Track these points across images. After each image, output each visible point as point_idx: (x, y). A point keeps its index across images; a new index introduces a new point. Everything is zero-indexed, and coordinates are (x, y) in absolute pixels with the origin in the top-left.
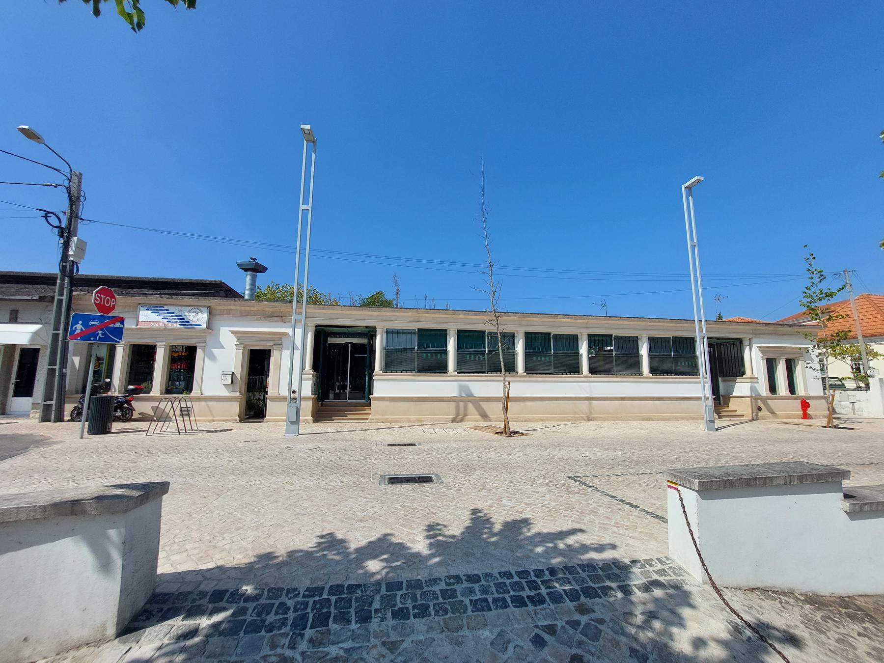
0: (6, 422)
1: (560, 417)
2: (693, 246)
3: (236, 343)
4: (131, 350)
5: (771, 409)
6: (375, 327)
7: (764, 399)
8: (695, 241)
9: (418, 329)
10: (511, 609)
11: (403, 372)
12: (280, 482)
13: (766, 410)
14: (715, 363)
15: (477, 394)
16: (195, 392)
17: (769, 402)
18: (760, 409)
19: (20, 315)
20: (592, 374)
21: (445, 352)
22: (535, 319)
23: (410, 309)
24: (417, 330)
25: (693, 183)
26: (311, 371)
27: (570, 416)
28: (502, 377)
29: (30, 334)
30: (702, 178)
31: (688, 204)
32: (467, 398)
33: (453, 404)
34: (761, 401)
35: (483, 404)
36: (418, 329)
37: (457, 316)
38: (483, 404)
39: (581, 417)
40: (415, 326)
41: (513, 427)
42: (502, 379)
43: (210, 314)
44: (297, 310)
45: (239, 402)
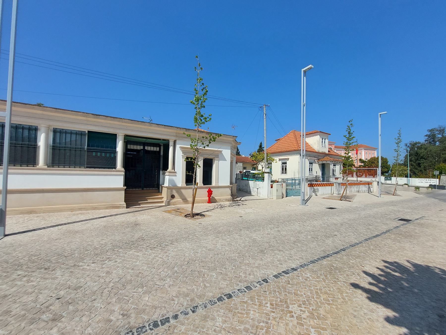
0: (145, 206)
2: (304, 105)
3: (182, 154)
5: (184, 196)
6: (168, 141)
7: (178, 189)
8: (305, 102)
9: (88, 131)
11: (61, 166)
13: (179, 197)
17: (183, 191)
18: (173, 197)
21: (115, 152)
23: (56, 109)
24: (87, 132)
25: (308, 68)
26: (123, 169)
30: (313, 67)
31: (304, 80)
34: (176, 190)
36: (88, 131)
40: (86, 128)
45: (124, 191)
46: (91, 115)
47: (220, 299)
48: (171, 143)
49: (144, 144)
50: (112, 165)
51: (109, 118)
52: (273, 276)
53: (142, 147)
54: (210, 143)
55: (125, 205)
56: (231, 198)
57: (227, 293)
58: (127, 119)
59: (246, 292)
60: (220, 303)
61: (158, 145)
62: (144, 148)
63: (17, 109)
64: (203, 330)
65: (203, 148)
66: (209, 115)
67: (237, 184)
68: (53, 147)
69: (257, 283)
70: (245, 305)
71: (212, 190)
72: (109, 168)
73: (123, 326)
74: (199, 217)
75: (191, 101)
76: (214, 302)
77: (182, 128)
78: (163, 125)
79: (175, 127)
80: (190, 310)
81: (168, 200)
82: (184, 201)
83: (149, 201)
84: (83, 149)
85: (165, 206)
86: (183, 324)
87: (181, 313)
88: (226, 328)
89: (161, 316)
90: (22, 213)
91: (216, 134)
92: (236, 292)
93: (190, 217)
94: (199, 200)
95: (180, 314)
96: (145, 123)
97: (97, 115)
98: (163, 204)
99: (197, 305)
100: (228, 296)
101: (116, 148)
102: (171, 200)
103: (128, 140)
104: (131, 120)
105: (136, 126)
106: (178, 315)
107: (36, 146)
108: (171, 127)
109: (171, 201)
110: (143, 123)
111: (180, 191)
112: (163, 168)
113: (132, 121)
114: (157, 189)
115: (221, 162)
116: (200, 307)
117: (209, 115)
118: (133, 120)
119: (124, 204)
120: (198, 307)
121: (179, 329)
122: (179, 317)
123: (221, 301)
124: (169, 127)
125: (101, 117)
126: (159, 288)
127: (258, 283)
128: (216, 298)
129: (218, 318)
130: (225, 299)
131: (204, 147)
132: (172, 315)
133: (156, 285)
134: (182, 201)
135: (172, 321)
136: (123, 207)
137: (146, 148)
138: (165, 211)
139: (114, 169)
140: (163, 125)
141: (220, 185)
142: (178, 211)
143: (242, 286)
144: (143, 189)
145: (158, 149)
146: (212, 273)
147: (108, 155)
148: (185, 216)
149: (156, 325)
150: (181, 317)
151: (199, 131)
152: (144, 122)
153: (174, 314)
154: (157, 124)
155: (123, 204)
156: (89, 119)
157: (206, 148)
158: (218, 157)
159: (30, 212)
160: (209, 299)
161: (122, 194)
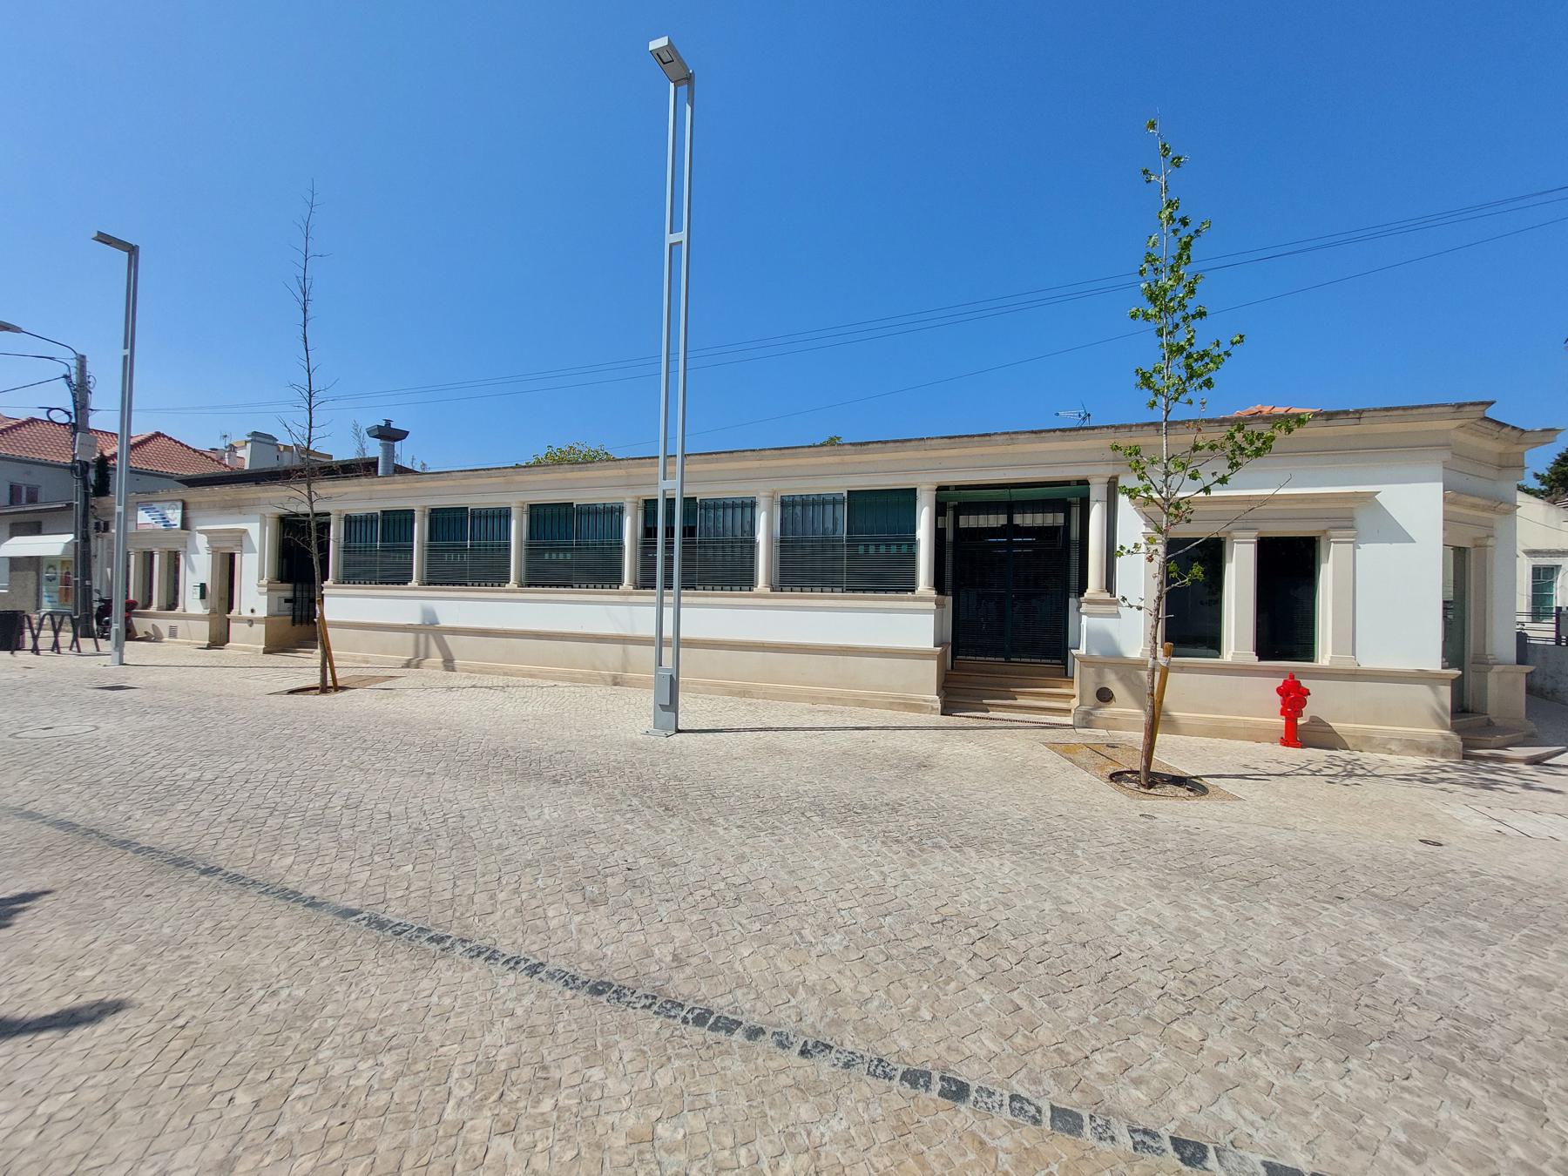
0: (1001, 717)
3: (1144, 529)
4: (1317, 553)
12: (1043, 860)
13: (1130, 700)
15: (445, 622)
16: (179, 610)
18: (1105, 696)
19: (43, 527)
20: (773, 590)
21: (913, 543)
22: (480, 481)
24: (845, 495)
26: (933, 593)
27: (581, 673)
28: (654, 595)
29: (63, 545)
32: (429, 629)
33: (410, 636)
34: (1117, 674)
35: (448, 638)
36: (382, 511)
38: (448, 638)
39: (600, 675)
40: (839, 485)
41: (1172, 754)
42: (654, 599)
43: (185, 507)
46: (850, 447)
47: (915, 1078)
48: (1097, 492)
49: (1010, 508)
50: (909, 586)
51: (892, 444)
52: (1264, 1164)
53: (1002, 520)
54: (1234, 465)
55: (938, 706)
57: (959, 1079)
58: (937, 438)
59: (1036, 1122)
60: (901, 1089)
61: (1062, 505)
62: (1010, 519)
63: (694, 467)
64: (768, 1112)
65: (1202, 494)
66: (1233, 343)
67: (1528, 669)
68: (781, 542)
69: (1133, 1131)
70: (972, 1156)
71: (1305, 683)
72: (897, 591)
73: (653, 979)
74: (1181, 791)
75: (1134, 309)
76: (887, 1070)
77: (1137, 425)
78: (1054, 431)
79: (1107, 427)
80: (802, 1043)
81: (1084, 708)
83: (1021, 701)
84: (838, 541)
85: (1073, 727)
86: (745, 1061)
87: (774, 1033)
88: (826, 1157)
89: (730, 1008)
90: (731, 692)
91: (1270, 419)
92: (997, 1098)
93: (1133, 785)
94: (1231, 725)
95: (768, 1035)
96: (993, 438)
97: (861, 444)
98: (1069, 720)
99: (831, 1043)
100: (954, 1089)
101: (914, 531)
103: (950, 502)
104: (950, 438)
106: (764, 1033)
107: (754, 542)
108: (1091, 432)
109: (1098, 712)
110: (988, 438)
112: (683, 574)
113: (952, 440)
114: (1059, 662)
115: (1367, 552)
116: (833, 1055)
117: (1233, 343)
118: (955, 437)
119: (936, 701)
120: (828, 1051)
121: (728, 1063)
122: (761, 1037)
123: (911, 1084)
125: (871, 446)
126: (796, 943)
127: (1135, 1131)
128: (907, 1066)
129: (841, 1116)
130: (932, 1087)
131: (1207, 490)
132: (753, 1024)
133: (800, 934)
135: (738, 1036)
136: (933, 709)
137: (1018, 519)
138: (1052, 746)
139: (909, 594)
140: (1054, 431)
141: (1367, 662)
142: (1109, 752)
143: (1052, 1094)
144: (1008, 660)
145: (1060, 519)
146: (980, 990)
147: (894, 549)
148: (1111, 776)
149: (700, 1020)
150: (767, 1042)
151: (1170, 424)
152: (989, 435)
153: (759, 1025)
154: (1033, 432)
155: (932, 701)
156: (847, 458)
157: (1213, 493)
158: (1350, 524)
159: (744, 693)
160: (884, 1053)
161: (928, 674)
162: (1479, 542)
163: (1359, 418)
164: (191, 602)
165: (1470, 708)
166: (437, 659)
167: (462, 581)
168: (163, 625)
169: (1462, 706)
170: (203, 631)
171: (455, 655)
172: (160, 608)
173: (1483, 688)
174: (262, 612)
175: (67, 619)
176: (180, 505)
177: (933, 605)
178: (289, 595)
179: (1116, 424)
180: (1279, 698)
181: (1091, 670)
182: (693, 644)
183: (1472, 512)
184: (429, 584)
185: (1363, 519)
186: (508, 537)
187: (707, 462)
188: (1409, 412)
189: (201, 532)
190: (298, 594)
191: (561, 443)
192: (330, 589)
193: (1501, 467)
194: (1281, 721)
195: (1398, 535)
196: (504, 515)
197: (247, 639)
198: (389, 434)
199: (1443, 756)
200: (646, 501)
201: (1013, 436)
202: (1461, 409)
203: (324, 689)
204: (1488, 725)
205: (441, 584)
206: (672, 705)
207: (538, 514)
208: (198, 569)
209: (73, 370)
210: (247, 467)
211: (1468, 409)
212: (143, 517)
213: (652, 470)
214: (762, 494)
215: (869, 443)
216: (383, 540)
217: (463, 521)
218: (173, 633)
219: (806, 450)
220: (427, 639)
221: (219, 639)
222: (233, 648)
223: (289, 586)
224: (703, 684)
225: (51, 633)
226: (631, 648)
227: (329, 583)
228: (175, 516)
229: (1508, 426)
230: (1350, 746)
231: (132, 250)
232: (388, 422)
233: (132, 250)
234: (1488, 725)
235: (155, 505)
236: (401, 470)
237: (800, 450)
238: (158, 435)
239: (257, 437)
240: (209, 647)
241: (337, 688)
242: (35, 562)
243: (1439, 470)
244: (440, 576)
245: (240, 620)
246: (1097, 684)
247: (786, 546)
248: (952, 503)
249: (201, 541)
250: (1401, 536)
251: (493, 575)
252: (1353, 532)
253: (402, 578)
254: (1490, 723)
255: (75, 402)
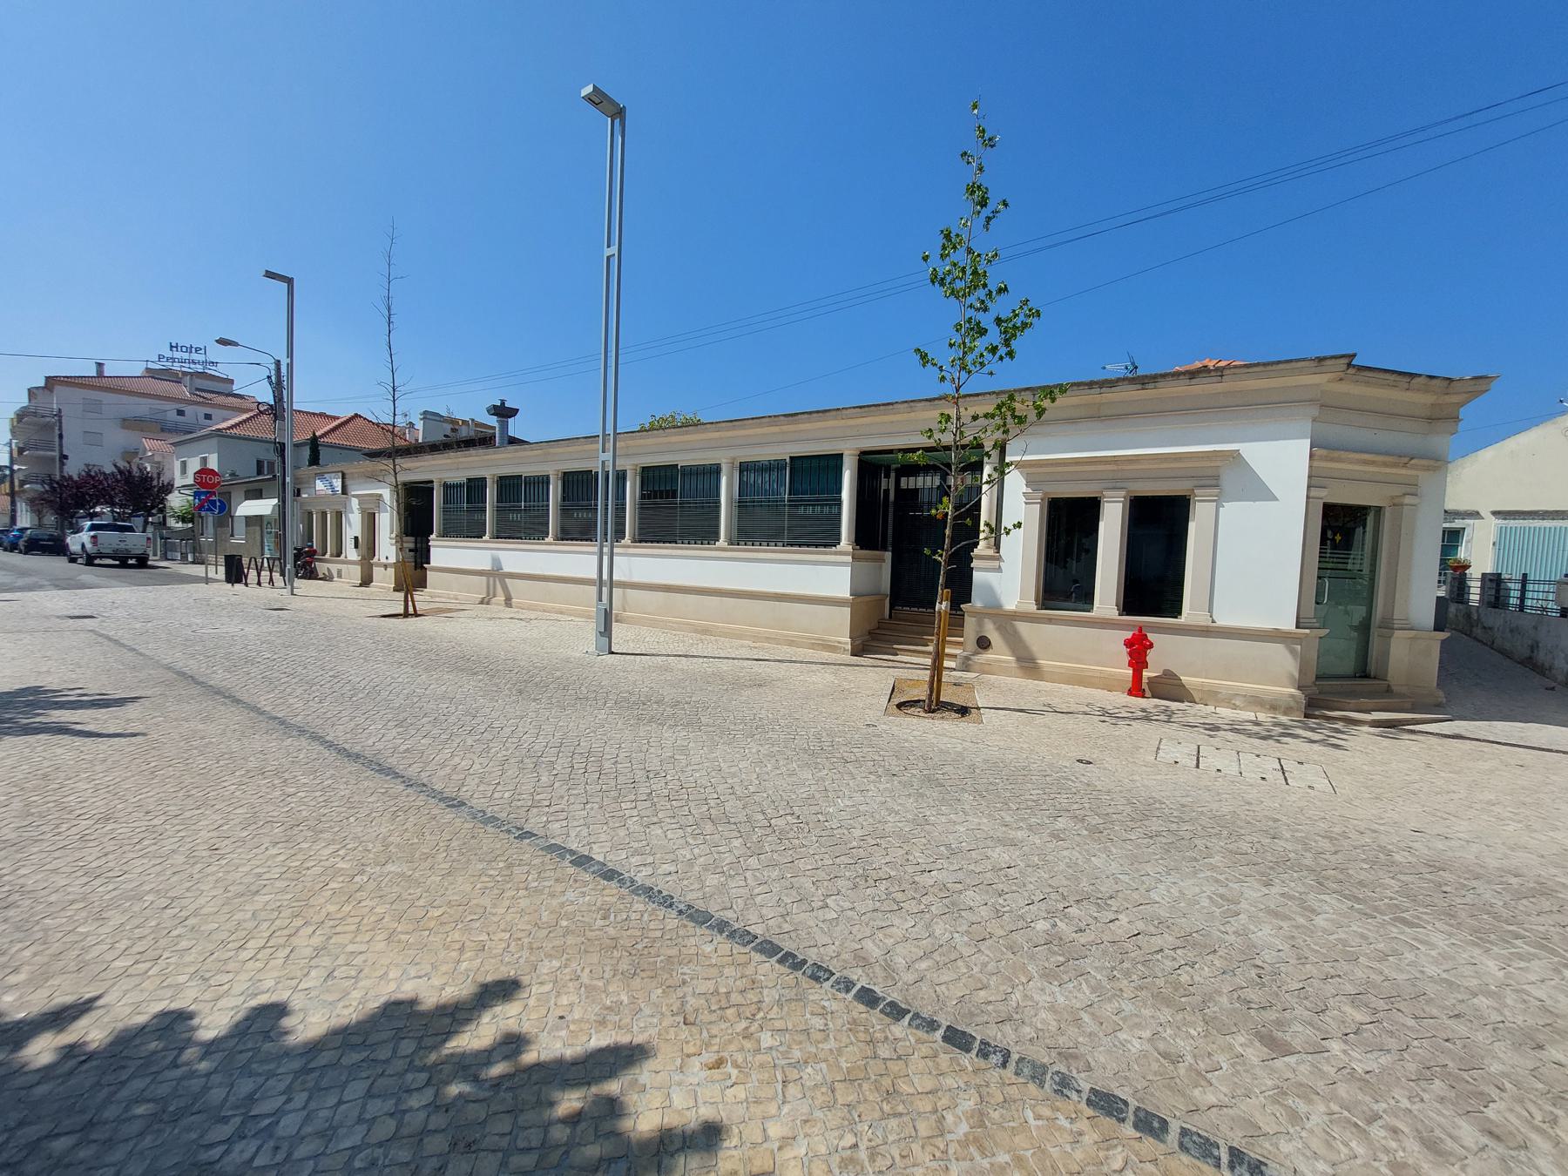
1: (582, 611)
3: (1025, 489)
5: (1026, 648)
10: (1129, 1130)
14: (606, 514)
15: (506, 569)
16: (342, 557)
17: (1023, 628)
18: (983, 644)
24: (788, 461)
32: (496, 575)
37: (489, 457)
40: (784, 452)
42: (596, 549)
43: (343, 478)
44: (1028, 396)
46: (782, 418)
56: (1292, 696)
71: (1151, 637)
72: (825, 546)
79: (989, 393)
82: (1023, 664)
94: (1090, 674)
96: (895, 406)
102: (976, 653)
103: (871, 466)
104: (861, 407)
105: (877, 419)
108: (976, 398)
109: (977, 658)
110: (891, 407)
111: (1013, 626)
113: (863, 410)
115: (1230, 510)
118: (864, 407)
124: (968, 399)
134: (1014, 665)
136: (845, 650)
141: (1223, 620)
154: (927, 400)
158: (1214, 482)
162: (1396, 501)
163: (1222, 376)
164: (351, 553)
165: (1372, 674)
166: (501, 598)
167: (519, 535)
168: (334, 568)
169: (1364, 671)
170: (356, 572)
171: (513, 595)
172: (332, 555)
173: (1386, 653)
174: (393, 560)
175: (277, 563)
176: (340, 474)
177: (849, 559)
178: (412, 546)
179: (996, 390)
180: (1125, 650)
181: (974, 619)
182: (624, 585)
183: (1357, 467)
184: (640, 542)
185: (1227, 479)
186: (718, 495)
187: (734, 428)
188: (1270, 368)
189: (354, 496)
190: (419, 545)
191: (663, 411)
192: (434, 541)
193: (1431, 419)
194: (1130, 671)
195: (1261, 492)
196: (715, 471)
197: (384, 579)
198: (503, 412)
199: (1285, 714)
200: (565, 473)
201: (912, 404)
202: (1323, 363)
203: (406, 615)
204: (1387, 691)
205: (652, 542)
206: (606, 632)
207: (650, 475)
208: (353, 526)
209: (273, 372)
210: (420, 441)
211: (1329, 362)
212: (320, 485)
213: (594, 446)
214: (724, 461)
215: (797, 414)
216: (790, 494)
217: (674, 479)
218: (340, 576)
219: (750, 421)
220: (495, 581)
221: (366, 581)
222: (376, 587)
223: (412, 539)
224: (676, 623)
225: (268, 573)
226: (629, 591)
227: (433, 536)
228: (338, 484)
229: (1420, 375)
230: (1197, 700)
231: (289, 281)
232: (503, 402)
233: (289, 281)
234: (1387, 691)
235: (326, 476)
236: (513, 441)
237: (745, 422)
238: (357, 416)
239: (426, 415)
240: (361, 585)
241: (416, 615)
242: (259, 518)
243: (1307, 426)
244: (506, 532)
245: (379, 565)
246: (977, 632)
247: (743, 505)
248: (894, 466)
249: (355, 503)
250: (1266, 495)
251: (704, 533)
252: (1216, 491)
253: (709, 535)
254: (1389, 691)
255: (274, 396)
